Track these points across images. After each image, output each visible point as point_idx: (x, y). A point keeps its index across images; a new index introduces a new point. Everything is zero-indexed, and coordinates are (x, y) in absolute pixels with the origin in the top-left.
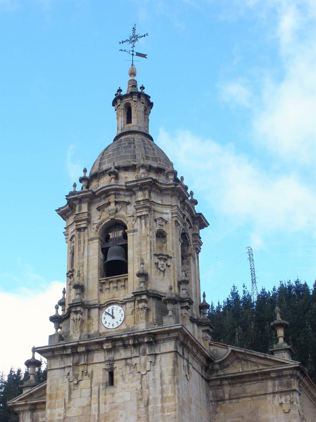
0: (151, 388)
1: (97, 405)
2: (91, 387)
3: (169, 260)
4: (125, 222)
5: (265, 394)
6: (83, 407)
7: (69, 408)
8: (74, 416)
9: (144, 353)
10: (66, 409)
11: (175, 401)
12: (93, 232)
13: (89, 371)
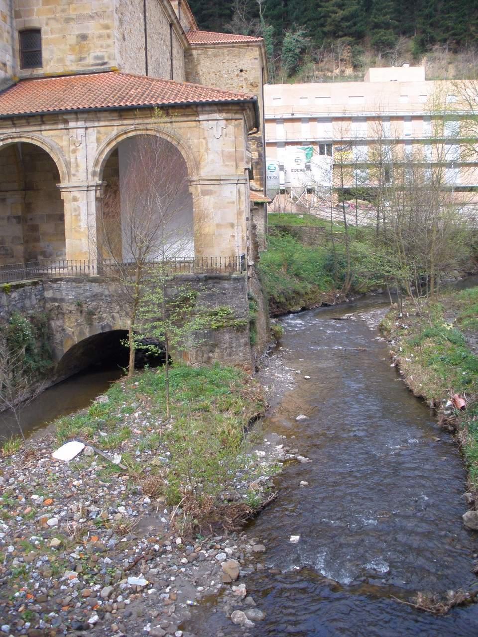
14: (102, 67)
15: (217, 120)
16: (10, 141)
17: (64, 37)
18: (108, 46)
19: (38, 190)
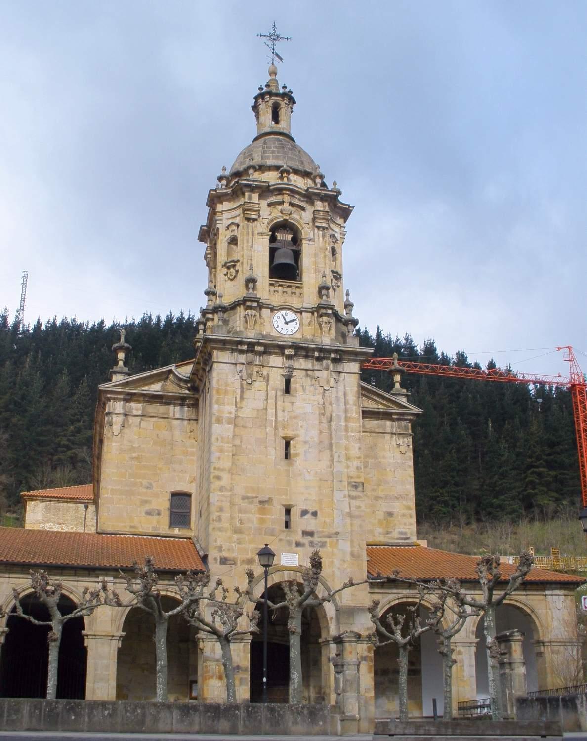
0: (333, 405)
1: (274, 410)
2: (267, 391)
4: (300, 228)
5: (384, 433)
6: (258, 410)
7: (241, 408)
8: (247, 418)
9: (327, 369)
10: (238, 407)
11: (359, 422)
12: (262, 227)
14: (406, 541)
15: (559, 595)
16: (404, 600)
17: (374, 512)
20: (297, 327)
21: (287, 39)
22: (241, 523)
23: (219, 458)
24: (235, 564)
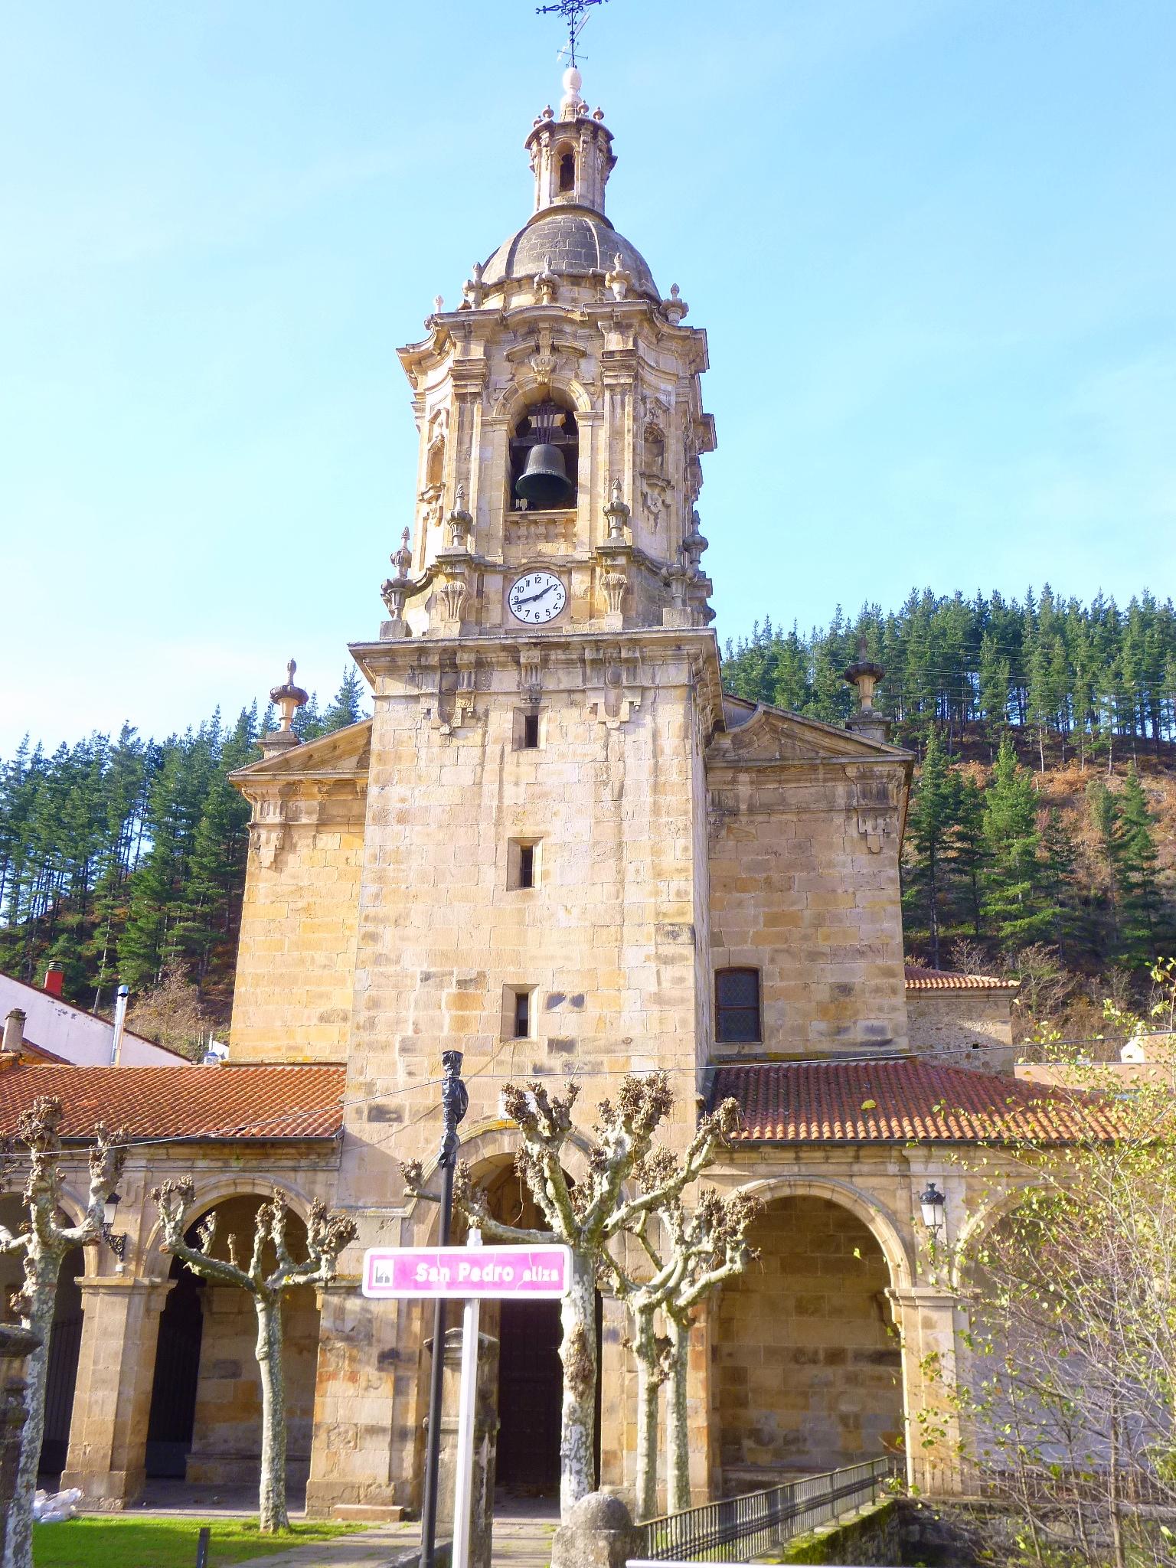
1: (497, 785)
2: (483, 746)
3: (669, 492)
13: (481, 709)
14: (883, 1049)
17: (806, 986)
18: (894, 1009)
19: (748, 1291)
20: (561, 603)
21: (545, 10)
22: (416, 1032)
23: (377, 896)
24: (399, 1119)
